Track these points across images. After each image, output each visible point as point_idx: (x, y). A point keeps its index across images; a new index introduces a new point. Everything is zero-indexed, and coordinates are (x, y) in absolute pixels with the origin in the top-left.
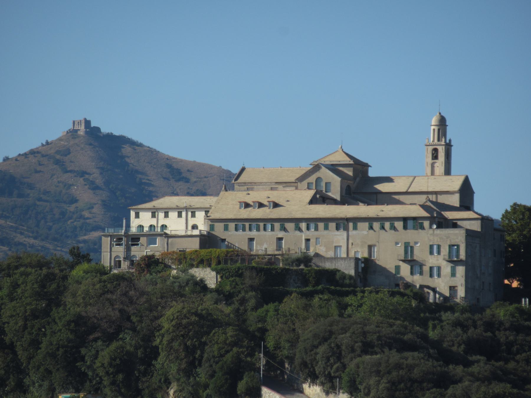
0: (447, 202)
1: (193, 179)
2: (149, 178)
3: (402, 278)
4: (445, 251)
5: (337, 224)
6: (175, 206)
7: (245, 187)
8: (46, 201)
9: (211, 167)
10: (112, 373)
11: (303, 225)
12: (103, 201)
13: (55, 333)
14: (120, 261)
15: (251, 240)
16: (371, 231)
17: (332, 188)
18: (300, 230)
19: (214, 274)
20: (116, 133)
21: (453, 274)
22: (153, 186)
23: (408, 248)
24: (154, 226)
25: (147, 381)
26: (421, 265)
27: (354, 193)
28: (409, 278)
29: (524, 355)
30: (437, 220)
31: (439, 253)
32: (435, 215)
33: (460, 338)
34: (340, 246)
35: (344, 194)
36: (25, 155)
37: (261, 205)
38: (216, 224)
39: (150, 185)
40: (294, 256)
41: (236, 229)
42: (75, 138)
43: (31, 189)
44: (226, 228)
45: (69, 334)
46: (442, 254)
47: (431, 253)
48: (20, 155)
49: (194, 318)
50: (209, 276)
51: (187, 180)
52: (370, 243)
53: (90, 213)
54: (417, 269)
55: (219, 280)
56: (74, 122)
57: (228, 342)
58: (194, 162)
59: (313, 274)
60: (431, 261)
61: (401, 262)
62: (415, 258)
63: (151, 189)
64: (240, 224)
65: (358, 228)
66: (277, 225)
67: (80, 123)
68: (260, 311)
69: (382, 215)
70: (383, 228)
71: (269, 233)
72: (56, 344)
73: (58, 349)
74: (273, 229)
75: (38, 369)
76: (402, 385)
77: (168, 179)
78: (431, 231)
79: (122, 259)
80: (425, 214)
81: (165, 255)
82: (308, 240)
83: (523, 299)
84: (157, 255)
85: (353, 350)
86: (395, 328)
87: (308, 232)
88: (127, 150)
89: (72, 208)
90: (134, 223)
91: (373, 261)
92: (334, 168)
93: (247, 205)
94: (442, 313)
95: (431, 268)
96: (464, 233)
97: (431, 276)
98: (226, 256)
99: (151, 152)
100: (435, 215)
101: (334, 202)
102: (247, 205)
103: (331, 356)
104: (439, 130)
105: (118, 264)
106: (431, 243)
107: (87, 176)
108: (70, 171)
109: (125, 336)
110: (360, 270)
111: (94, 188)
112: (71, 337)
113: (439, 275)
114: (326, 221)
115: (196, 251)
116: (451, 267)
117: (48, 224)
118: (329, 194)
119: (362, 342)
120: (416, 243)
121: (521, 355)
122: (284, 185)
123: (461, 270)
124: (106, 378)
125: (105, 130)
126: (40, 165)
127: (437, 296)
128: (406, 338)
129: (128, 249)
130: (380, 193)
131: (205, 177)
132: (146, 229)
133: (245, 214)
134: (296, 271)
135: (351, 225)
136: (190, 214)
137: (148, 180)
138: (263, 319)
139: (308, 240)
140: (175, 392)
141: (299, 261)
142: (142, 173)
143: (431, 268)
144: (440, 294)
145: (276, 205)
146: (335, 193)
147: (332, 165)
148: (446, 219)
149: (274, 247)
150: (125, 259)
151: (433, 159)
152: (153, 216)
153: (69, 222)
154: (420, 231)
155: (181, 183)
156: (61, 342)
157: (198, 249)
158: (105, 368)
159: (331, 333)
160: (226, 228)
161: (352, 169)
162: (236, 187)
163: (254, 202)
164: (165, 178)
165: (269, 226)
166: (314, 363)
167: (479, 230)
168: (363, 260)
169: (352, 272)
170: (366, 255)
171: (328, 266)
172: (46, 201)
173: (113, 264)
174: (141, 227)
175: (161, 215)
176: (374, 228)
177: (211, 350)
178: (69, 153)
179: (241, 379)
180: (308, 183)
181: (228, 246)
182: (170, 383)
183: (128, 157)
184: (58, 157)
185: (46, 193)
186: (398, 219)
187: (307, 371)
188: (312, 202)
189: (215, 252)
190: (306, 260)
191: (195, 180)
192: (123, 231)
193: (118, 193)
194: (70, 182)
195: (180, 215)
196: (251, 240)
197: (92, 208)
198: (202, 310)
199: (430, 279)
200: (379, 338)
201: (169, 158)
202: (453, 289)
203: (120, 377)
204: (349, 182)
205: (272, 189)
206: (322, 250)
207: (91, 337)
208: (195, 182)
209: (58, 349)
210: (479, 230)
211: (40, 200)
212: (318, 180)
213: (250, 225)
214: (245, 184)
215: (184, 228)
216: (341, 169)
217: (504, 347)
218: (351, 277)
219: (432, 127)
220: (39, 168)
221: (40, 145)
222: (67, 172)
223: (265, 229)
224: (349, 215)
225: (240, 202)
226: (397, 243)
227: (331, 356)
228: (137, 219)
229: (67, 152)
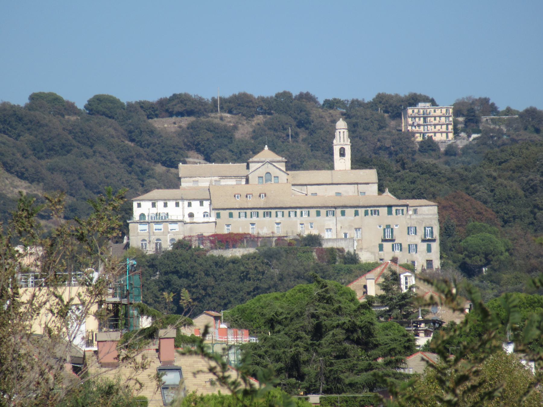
4: (421, 233)
21: (429, 250)
38: (222, 212)
96: (434, 214)
106: (409, 226)
121: (491, 226)
123: (436, 246)
152: (154, 205)
171: (335, 245)
195: (177, 205)
202: (430, 263)
223: (277, 216)
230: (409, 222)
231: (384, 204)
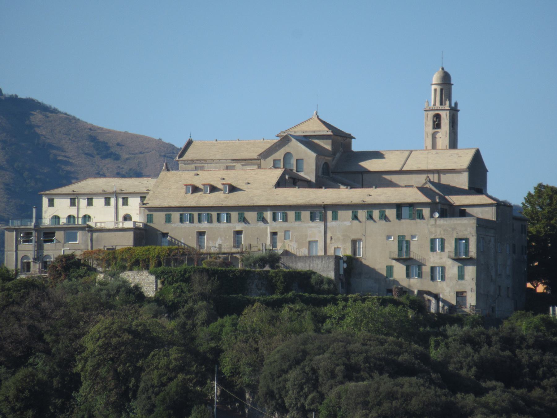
1: (125, 156)
2: (67, 154)
3: (395, 282)
4: (450, 246)
5: (311, 213)
6: (100, 191)
9: (148, 140)
10: (19, 409)
11: (268, 215)
14: (28, 264)
15: (201, 234)
16: (356, 222)
17: (305, 166)
18: (264, 220)
19: (152, 278)
20: (22, 95)
21: (461, 276)
22: (71, 164)
24: (74, 217)
30: (439, 206)
31: (442, 249)
33: (470, 358)
34: (316, 242)
37: (213, 189)
39: (67, 163)
40: (257, 255)
41: (182, 221)
44: (168, 219)
46: (446, 250)
47: (433, 249)
49: (127, 337)
52: (354, 237)
54: (415, 270)
55: (160, 286)
58: (126, 133)
60: (432, 260)
61: (394, 261)
62: (412, 256)
63: (69, 168)
64: (187, 213)
66: (235, 215)
69: (369, 200)
70: (370, 217)
71: (224, 224)
74: (229, 220)
77: (92, 156)
78: (432, 221)
79: (31, 260)
80: (424, 199)
82: (274, 234)
83: (551, 308)
84: (79, 254)
85: (333, 376)
86: (386, 346)
87: (274, 224)
88: (37, 117)
90: (48, 213)
93: (195, 189)
94: (447, 326)
95: (433, 269)
97: (433, 278)
98: (169, 255)
99: (70, 120)
100: (438, 200)
101: (308, 184)
102: (195, 189)
103: (305, 383)
104: (442, 90)
105: (27, 267)
106: (433, 237)
109: (37, 360)
110: (342, 272)
113: (443, 278)
114: (298, 208)
115: (129, 249)
116: (459, 267)
119: (344, 364)
120: (413, 237)
122: (244, 163)
123: (471, 271)
127: (441, 304)
128: (400, 359)
129: (39, 248)
130: (369, 172)
131: (141, 153)
132: (63, 221)
135: (329, 214)
136: (120, 201)
138: (216, 337)
139: (274, 234)
141: (263, 261)
143: (433, 269)
144: (444, 301)
145: (233, 189)
146: (308, 172)
147: (305, 136)
148: (451, 205)
150: (36, 260)
152: (73, 204)
155: (108, 160)
157: (132, 247)
159: (305, 353)
160: (168, 219)
161: (330, 141)
162: (181, 165)
164: (87, 154)
165: (224, 216)
166: (283, 393)
168: (345, 259)
169: (332, 275)
170: (349, 253)
171: (301, 267)
173: (19, 267)
174: (56, 218)
175: (83, 202)
176: (359, 217)
180: (274, 161)
181: (170, 243)
183: (39, 127)
187: (274, 402)
188: (279, 184)
189: (155, 250)
191: (126, 156)
192: (33, 224)
193: (26, 174)
195: (107, 203)
196: (201, 234)
199: (431, 282)
200: (367, 360)
201: (92, 128)
202: (460, 295)
205: (227, 168)
206: (292, 247)
208: (127, 159)
212: (287, 156)
213: (199, 215)
214: (192, 161)
216: (316, 141)
217: (527, 370)
218: (330, 281)
219: (433, 87)
223: (219, 220)
224: (328, 201)
225: (186, 185)
226: (388, 237)
227: (305, 383)
228: (51, 208)
230: (433, 230)
231: (494, 196)
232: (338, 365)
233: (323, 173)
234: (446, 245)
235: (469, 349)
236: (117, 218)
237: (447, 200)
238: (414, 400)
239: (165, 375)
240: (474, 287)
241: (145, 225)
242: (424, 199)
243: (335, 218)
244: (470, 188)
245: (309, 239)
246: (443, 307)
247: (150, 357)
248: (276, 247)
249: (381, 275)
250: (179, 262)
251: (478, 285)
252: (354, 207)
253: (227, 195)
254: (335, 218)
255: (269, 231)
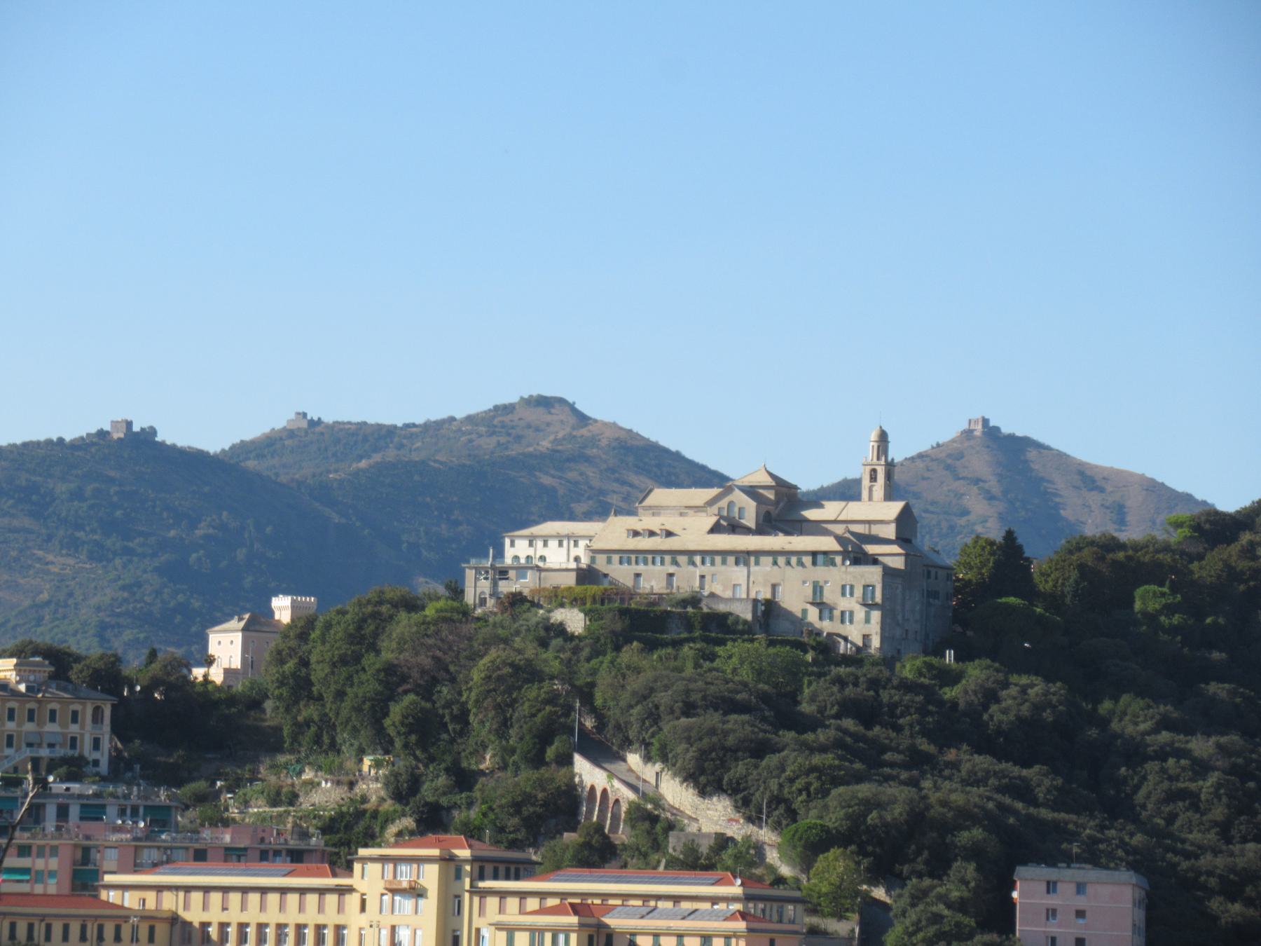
0: (882, 535)
1: (1109, 489)
2: (1056, 487)
3: (810, 624)
4: (858, 592)
5: (736, 558)
6: (555, 534)
7: (651, 512)
8: (932, 513)
9: (1132, 474)
10: (404, 733)
11: (698, 559)
12: (1000, 514)
13: (363, 683)
14: (485, 599)
15: (638, 575)
16: (776, 567)
17: (746, 515)
18: (693, 564)
19: (582, 615)
20: (1019, 433)
21: (867, 620)
22: (1061, 496)
23: (818, 589)
24: (532, 558)
25: (462, 743)
26: (831, 609)
27: (776, 520)
28: (818, 625)
29: (908, 718)
30: (852, 555)
31: (852, 594)
32: (850, 549)
33: (833, 698)
34: (740, 585)
35: (761, 522)
36: (912, 459)
37: (652, 534)
39: (1056, 495)
40: (680, 597)
41: (621, 563)
42: (970, 439)
43: (917, 499)
44: (609, 561)
45: (377, 685)
46: (855, 595)
47: (843, 594)
48: (906, 459)
49: (508, 670)
50: (577, 618)
51: (1102, 490)
52: (774, 581)
53: (984, 527)
54: (826, 613)
55: (588, 623)
56: (970, 421)
57: (540, 699)
58: (1112, 468)
59: (699, 618)
60: (842, 604)
61: (809, 605)
62: (825, 600)
63: (1058, 500)
64: (625, 556)
65: (761, 563)
66: (668, 558)
67: (976, 421)
68: (594, 662)
69: (788, 548)
70: (788, 563)
71: (658, 567)
72: (363, 697)
73: (364, 702)
74: (662, 563)
75: (346, 726)
76: (714, 754)
77: (1078, 488)
78: (843, 568)
79: (487, 596)
80: (837, 547)
81: (539, 591)
82: (702, 577)
83: (948, 652)
84: (526, 592)
85: (672, 712)
86: (731, 685)
87: (703, 567)
88: (1032, 454)
89: (963, 521)
90: (509, 553)
91: (776, 603)
92: (751, 491)
93: (636, 534)
94: (833, 667)
95: (843, 613)
97: (843, 621)
98: (604, 594)
99: (1061, 456)
100: (850, 549)
101: (747, 531)
102: (636, 534)
103: (647, 718)
104: (879, 447)
105: (483, 602)
106: (844, 583)
107: (981, 484)
108: (963, 478)
109: (444, 688)
110: (759, 614)
111: (991, 498)
112: (380, 688)
113: (851, 622)
114: (724, 554)
115: (570, 588)
116: (866, 612)
117: (934, 540)
118: (742, 521)
119: (683, 701)
120: (826, 582)
122: (696, 510)
123: (876, 615)
124: (397, 740)
125: (1006, 429)
126: (928, 470)
127: (849, 646)
128: (739, 697)
129: (495, 585)
130: (808, 521)
131: (1124, 486)
132: (523, 561)
133: (645, 543)
134: (679, 614)
135: (752, 559)
136: (572, 543)
137: (1056, 489)
138: (594, 672)
139: (702, 577)
140: (491, 757)
141: (684, 602)
142: (1049, 482)
143: (843, 613)
144: (852, 643)
145: (669, 534)
146: (750, 520)
147: (751, 487)
148: (865, 554)
149: (664, 584)
150: (491, 595)
151: (871, 482)
152: (531, 545)
153: (958, 538)
154: (831, 567)
155: (1093, 493)
156: (368, 695)
157: (573, 586)
158: (396, 727)
159: (652, 690)
160: (609, 561)
161: (773, 492)
162: (640, 511)
163: (644, 530)
164: (1074, 487)
165: (658, 559)
166: (629, 726)
167: (903, 567)
168: (763, 602)
169: (749, 617)
170: (769, 596)
171: (722, 608)
172: (932, 513)
173: (477, 601)
174: (516, 558)
175: (540, 544)
176: (779, 563)
177: (524, 709)
178: (962, 457)
179: (551, 743)
180: (719, 508)
181: (611, 583)
182: (487, 747)
183: (1032, 461)
184: (949, 461)
185: (933, 503)
186: (806, 553)
187: (621, 735)
188: (715, 529)
189: (593, 589)
190: (694, 600)
191: (1111, 489)
192: (490, 563)
193: (1018, 504)
194: (962, 491)
195: (561, 544)
196: (638, 575)
197: (986, 521)
198: (520, 660)
199: (841, 626)
200: (704, 698)
201: (1081, 464)
202: (866, 637)
203: (413, 738)
204: (769, 507)
205: (681, 514)
206: (718, 589)
207: (400, 690)
208: (1112, 492)
209: (364, 702)
210: (903, 567)
211: (926, 511)
212: (731, 504)
213: (637, 558)
214: (650, 507)
215: (564, 559)
216: (761, 491)
217: (886, 709)
218: (745, 622)
219: (872, 444)
220: (927, 475)
221: (930, 447)
222: (958, 479)
223: (654, 563)
224: (752, 547)
225: (628, 530)
226: (804, 582)
227: (647, 718)
228: (512, 549)
229: (960, 456)
230: (844, 576)
232: (677, 702)
233: (764, 521)
234: (855, 591)
235: (835, 689)
236: (568, 560)
237: (862, 549)
238: (731, 735)
239: (535, 707)
240: (879, 630)
241: (589, 566)
242: (837, 547)
243: (757, 563)
244: (897, 538)
245: (733, 583)
246: (851, 648)
247: (523, 690)
248: (704, 589)
249: (797, 617)
250: (611, 600)
251: (882, 629)
252: (774, 554)
253: (664, 539)
254: (757, 563)
255: (698, 574)
